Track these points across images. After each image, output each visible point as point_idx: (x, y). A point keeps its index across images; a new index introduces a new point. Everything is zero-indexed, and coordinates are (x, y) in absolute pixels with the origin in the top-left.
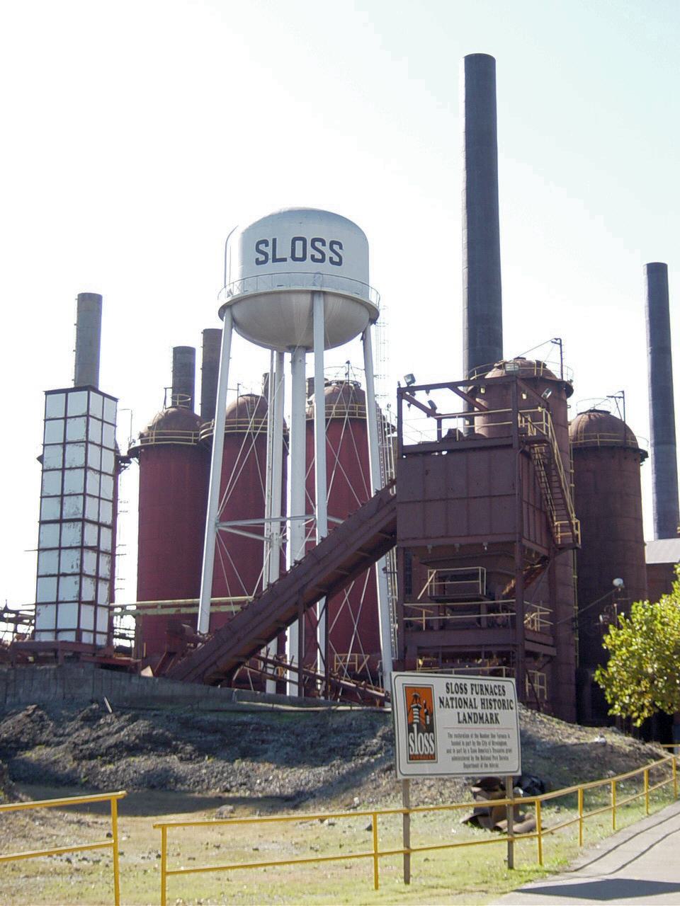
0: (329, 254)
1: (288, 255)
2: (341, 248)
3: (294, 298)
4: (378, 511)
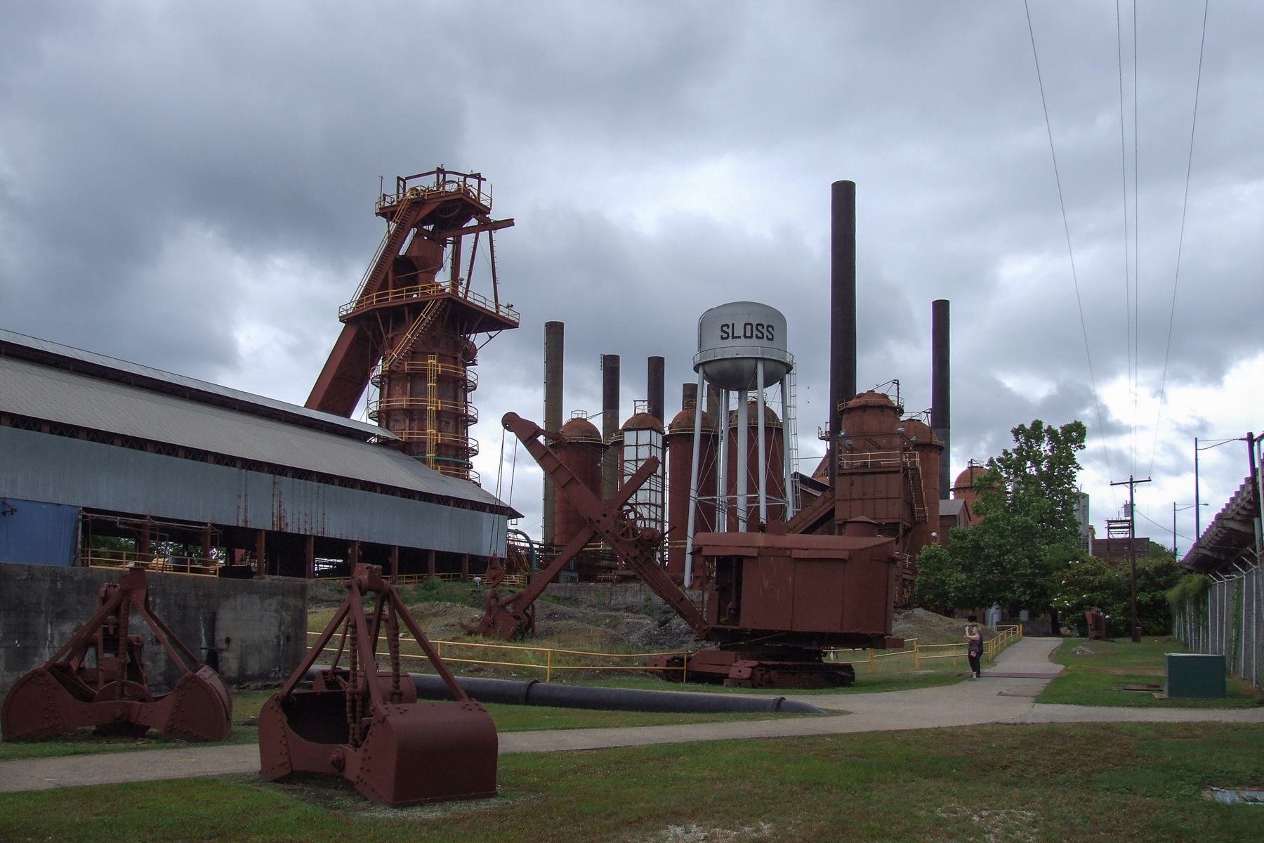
0: (766, 333)
1: (742, 334)
3: (745, 363)
4: (823, 504)
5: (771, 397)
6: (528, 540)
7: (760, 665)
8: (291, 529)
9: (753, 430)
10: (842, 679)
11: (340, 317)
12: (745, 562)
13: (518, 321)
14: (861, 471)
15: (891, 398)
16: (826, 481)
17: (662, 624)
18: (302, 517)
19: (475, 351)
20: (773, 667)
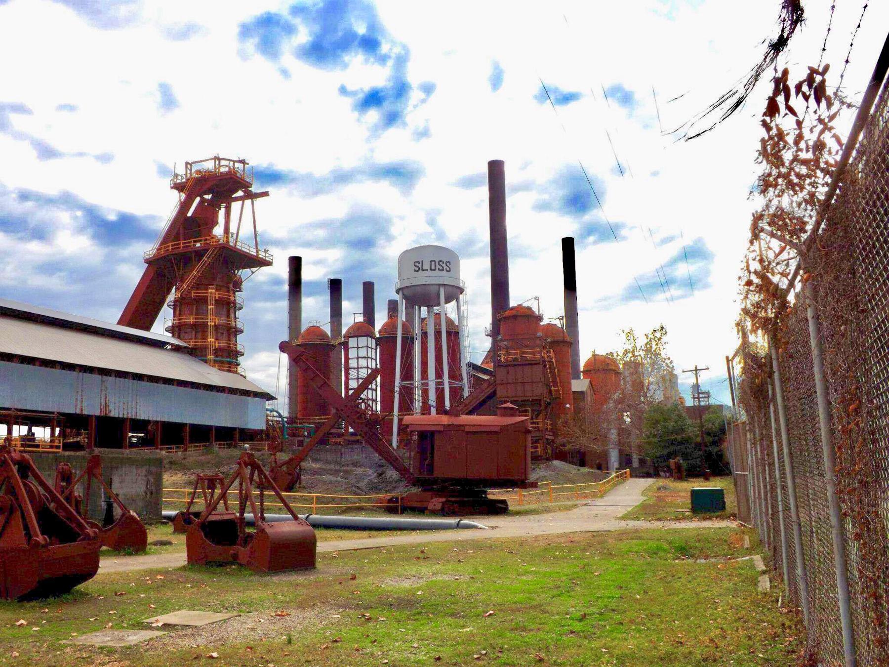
0: (445, 267)
5: (450, 309)
6: (280, 416)
7: (446, 501)
8: (114, 414)
9: (438, 333)
10: (499, 509)
12: (436, 437)
14: (514, 363)
16: (490, 367)
17: (380, 475)
18: (121, 404)
19: (242, 282)
20: (456, 502)
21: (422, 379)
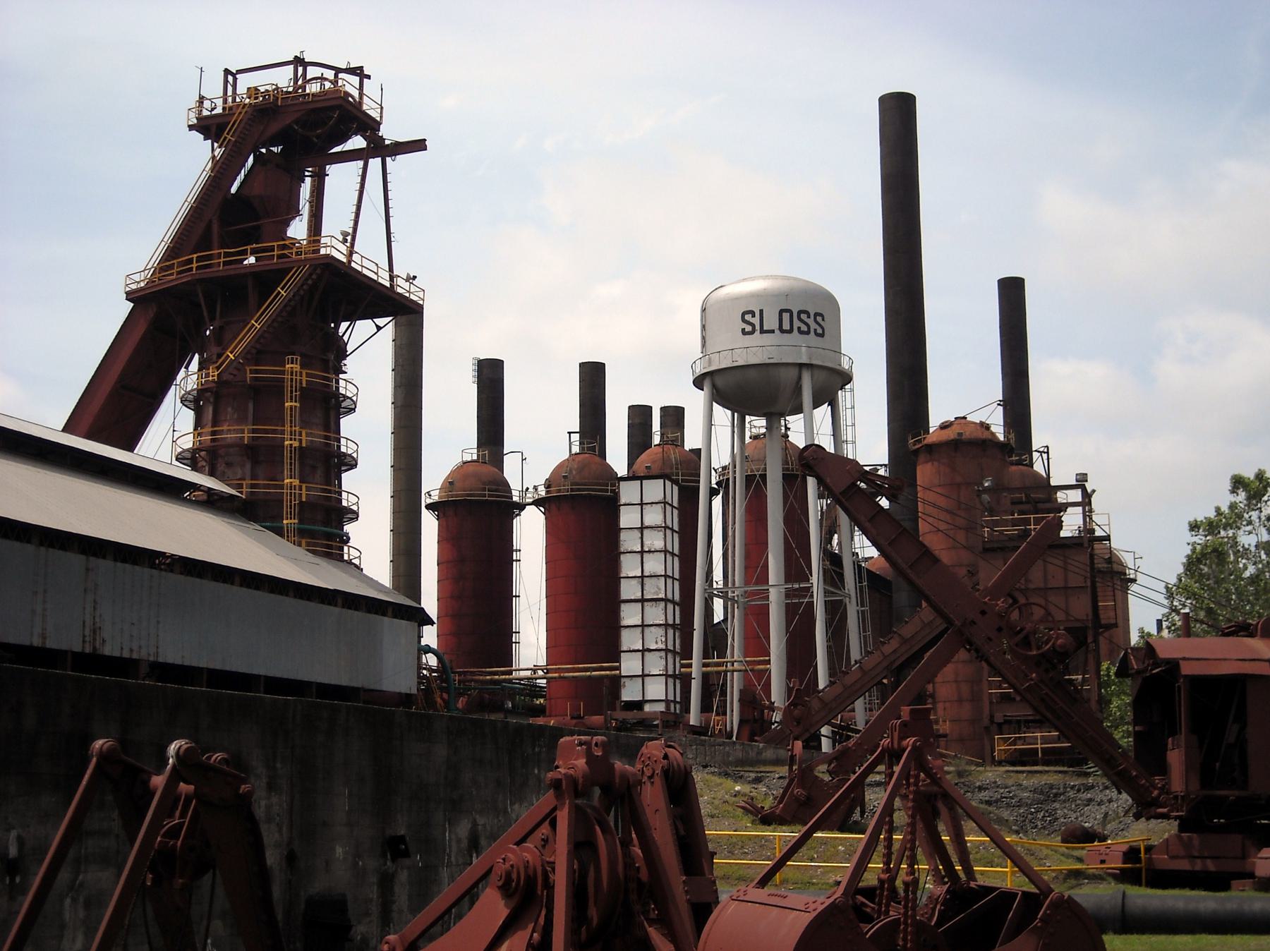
0: (813, 326)
1: (775, 326)
2: (823, 320)
3: (783, 371)
11: (127, 293)
13: (421, 302)
15: (993, 429)
21: (788, 578)
